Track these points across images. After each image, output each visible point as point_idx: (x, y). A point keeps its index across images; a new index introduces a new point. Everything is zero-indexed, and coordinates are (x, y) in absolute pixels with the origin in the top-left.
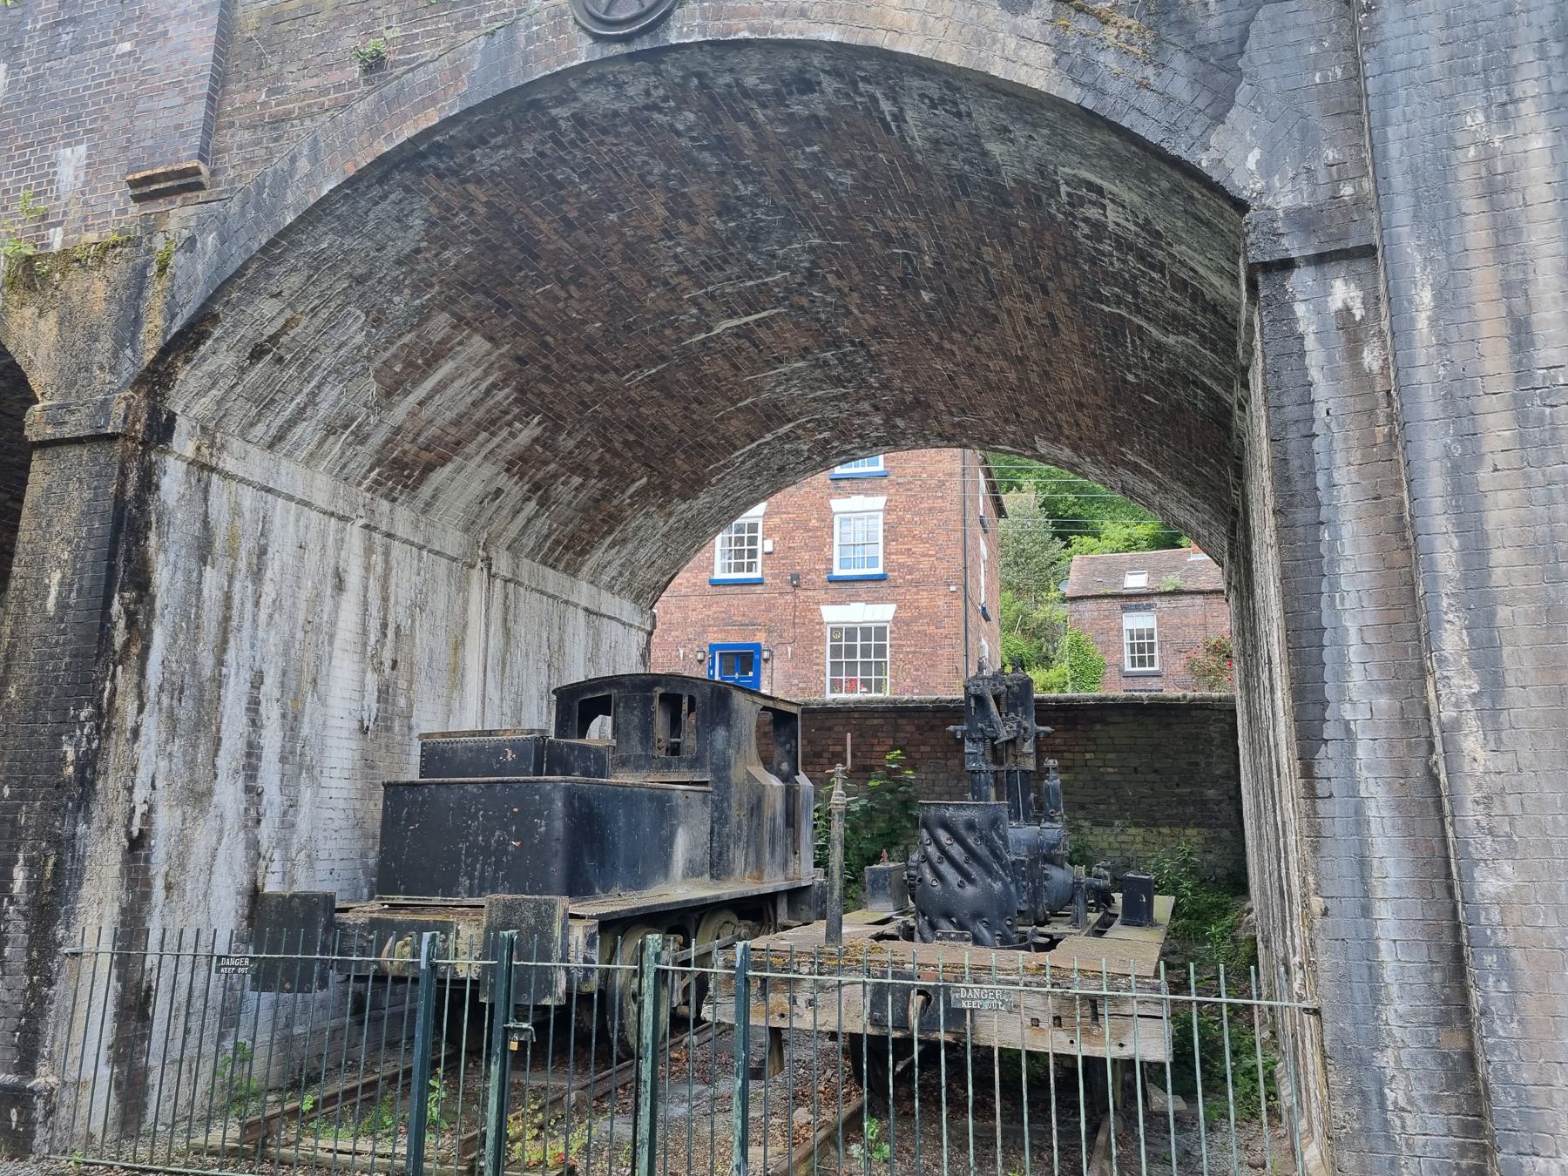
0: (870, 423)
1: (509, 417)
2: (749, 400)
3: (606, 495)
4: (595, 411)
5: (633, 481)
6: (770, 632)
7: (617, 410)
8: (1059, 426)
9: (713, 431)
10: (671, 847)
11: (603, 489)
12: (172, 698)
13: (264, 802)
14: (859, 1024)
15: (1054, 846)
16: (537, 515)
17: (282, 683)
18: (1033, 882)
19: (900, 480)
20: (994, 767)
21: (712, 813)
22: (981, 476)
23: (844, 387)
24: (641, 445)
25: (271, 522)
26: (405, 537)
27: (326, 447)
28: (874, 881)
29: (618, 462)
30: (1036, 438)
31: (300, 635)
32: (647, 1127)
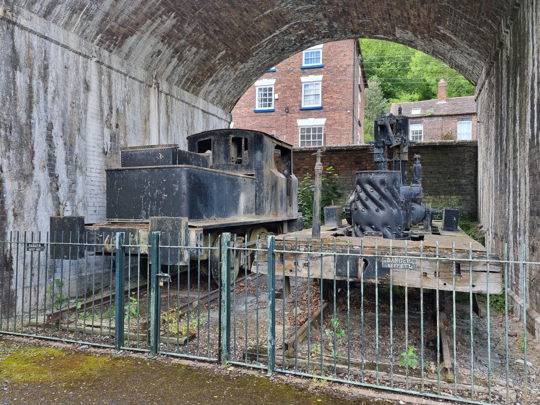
0: (322, 25)
1: (160, 12)
2: (269, 11)
3: (208, 58)
4: (200, 13)
5: (219, 52)
6: (277, 130)
7: (210, 13)
8: (409, 19)
9: (254, 28)
10: (238, 201)
11: (206, 55)
12: (6, 131)
13: (60, 181)
14: (330, 275)
15: (417, 195)
16: (178, 65)
17: (63, 130)
18: (407, 211)
19: (329, 68)
20: (388, 160)
21: (256, 188)
22: (360, 69)
23: (312, 4)
24: (222, 33)
25: (49, 54)
26: (117, 69)
27: (73, 20)
28: (328, 214)
29: (212, 41)
30: (396, 28)
31: (69, 108)
32: (226, 322)
